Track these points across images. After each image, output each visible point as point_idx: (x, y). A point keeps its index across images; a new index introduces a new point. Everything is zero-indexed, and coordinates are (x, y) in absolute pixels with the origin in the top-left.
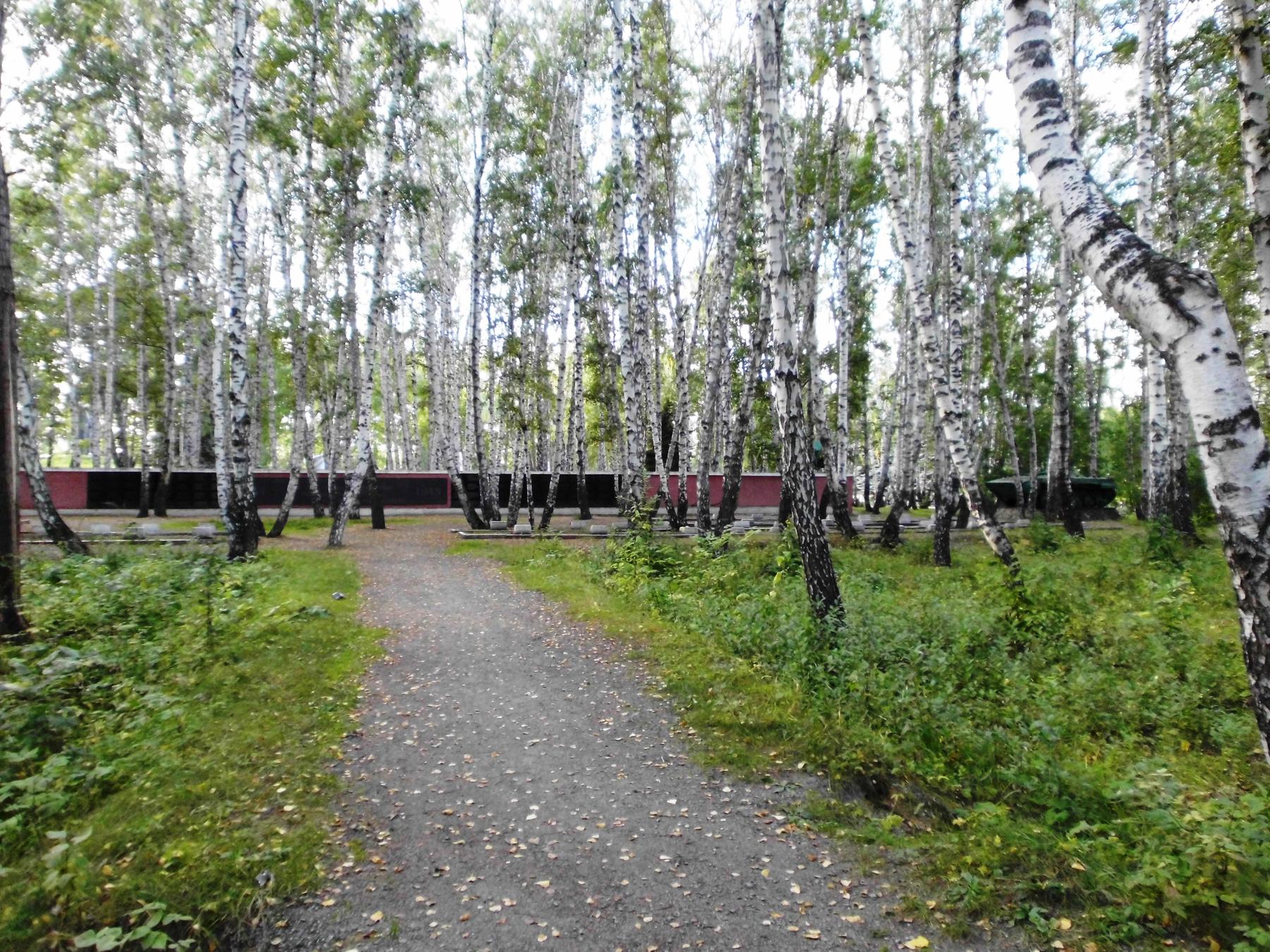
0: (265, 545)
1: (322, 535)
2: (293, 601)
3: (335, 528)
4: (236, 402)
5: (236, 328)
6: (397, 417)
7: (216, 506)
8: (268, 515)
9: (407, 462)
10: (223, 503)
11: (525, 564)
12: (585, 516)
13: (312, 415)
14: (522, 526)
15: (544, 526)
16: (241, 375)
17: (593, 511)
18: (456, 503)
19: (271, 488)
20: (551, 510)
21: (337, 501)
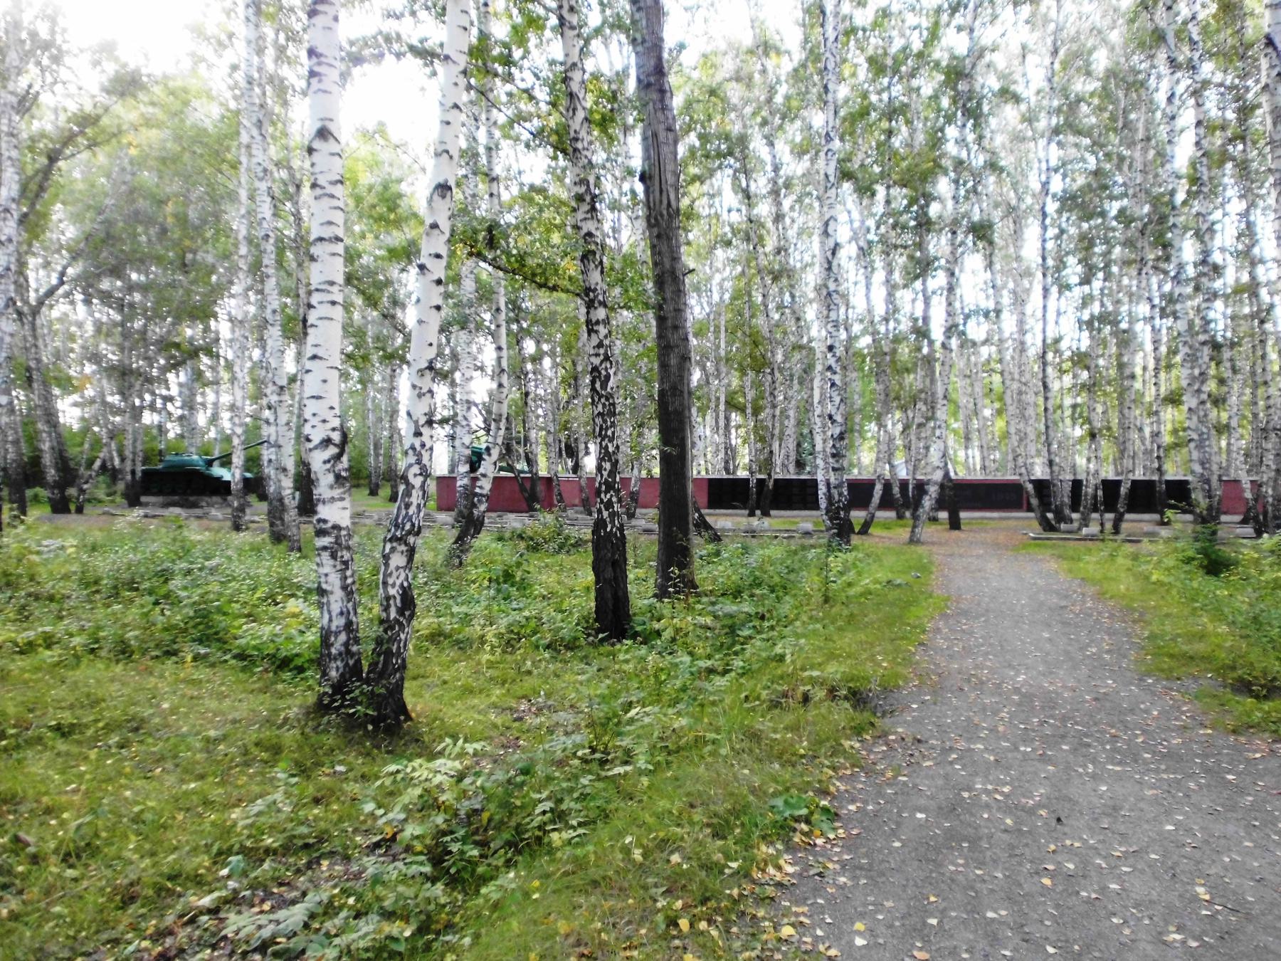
0: (855, 540)
1: (904, 533)
2: (882, 575)
3: (914, 527)
4: (833, 422)
6: (975, 424)
7: (817, 508)
8: (858, 516)
9: (984, 468)
10: (823, 503)
11: (1079, 560)
13: (894, 423)
15: (1116, 530)
16: (837, 399)
18: (1030, 509)
19: (860, 492)
20: (1122, 515)
21: (917, 504)
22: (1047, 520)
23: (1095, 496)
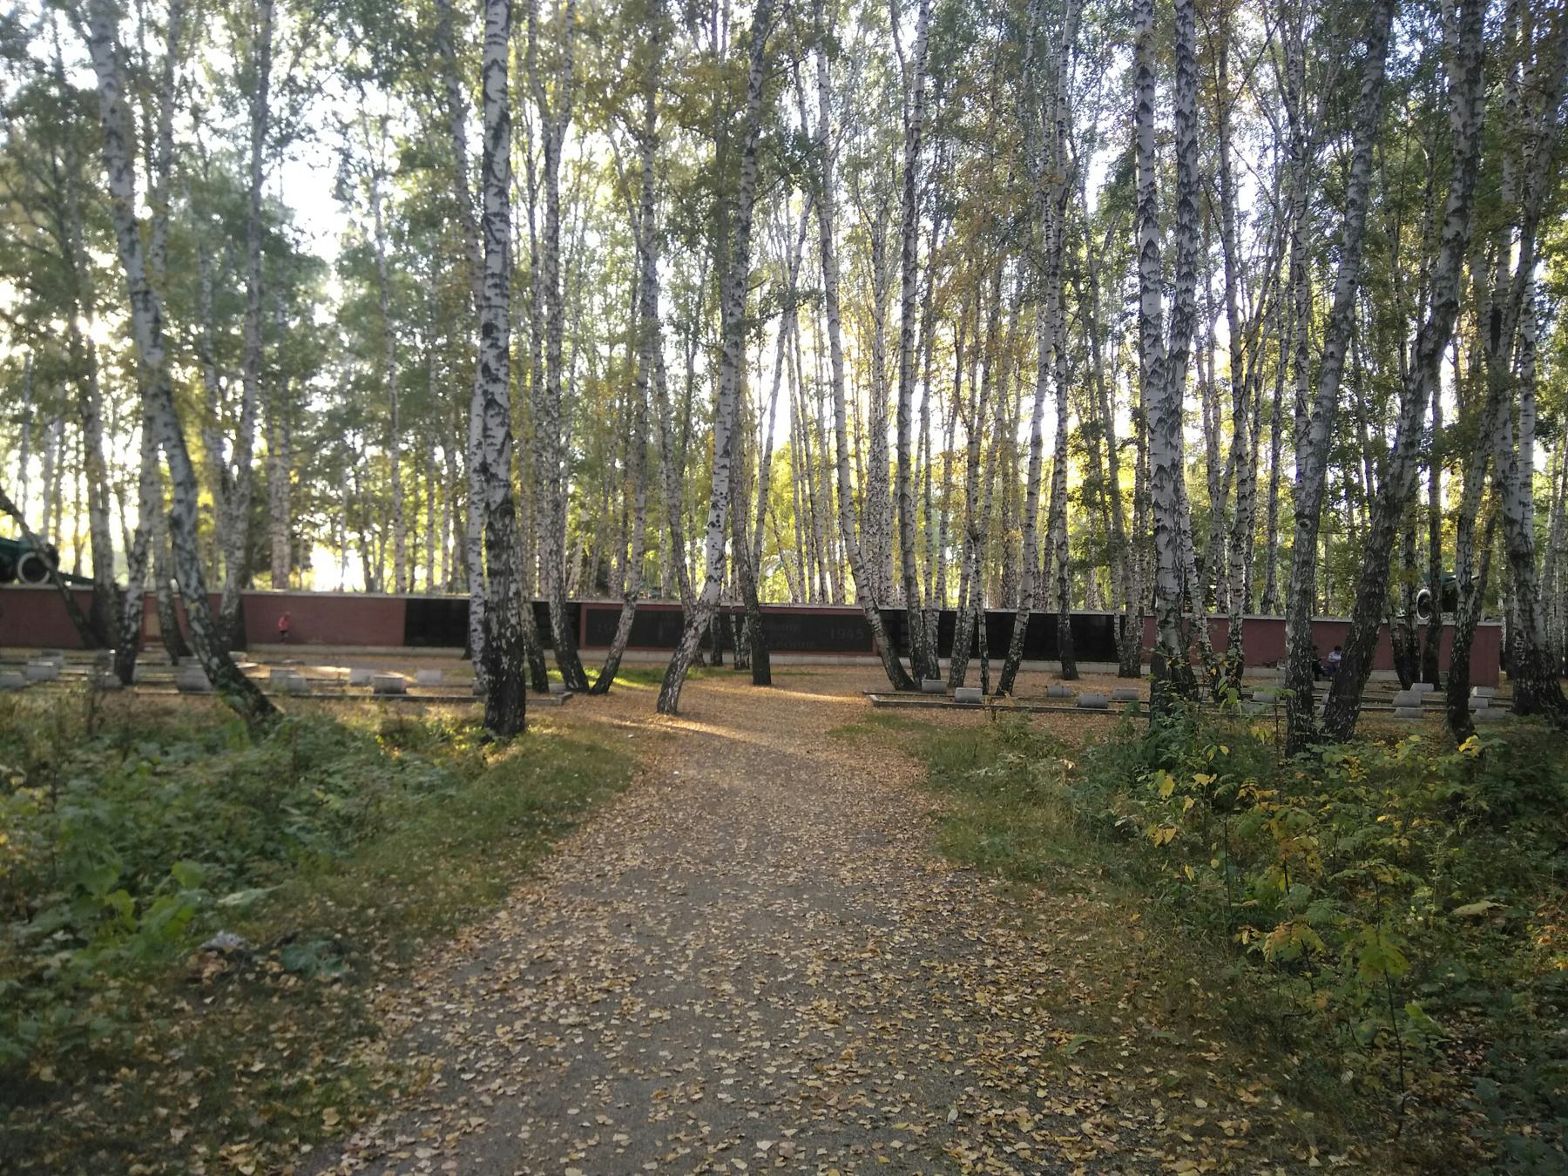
5: (490, 357)
10: (478, 644)
12: (1069, 674)
14: (971, 687)
15: (1006, 685)
17: (1081, 667)
22: (900, 668)
23: (976, 634)
